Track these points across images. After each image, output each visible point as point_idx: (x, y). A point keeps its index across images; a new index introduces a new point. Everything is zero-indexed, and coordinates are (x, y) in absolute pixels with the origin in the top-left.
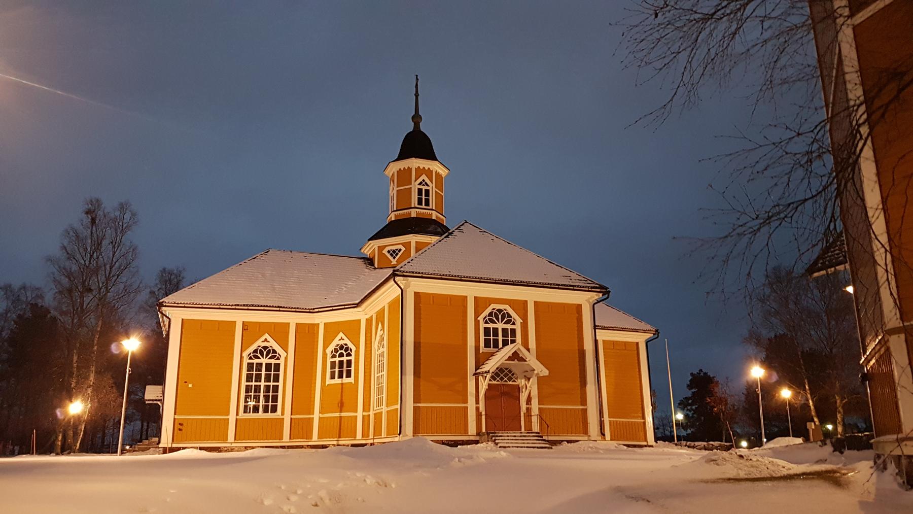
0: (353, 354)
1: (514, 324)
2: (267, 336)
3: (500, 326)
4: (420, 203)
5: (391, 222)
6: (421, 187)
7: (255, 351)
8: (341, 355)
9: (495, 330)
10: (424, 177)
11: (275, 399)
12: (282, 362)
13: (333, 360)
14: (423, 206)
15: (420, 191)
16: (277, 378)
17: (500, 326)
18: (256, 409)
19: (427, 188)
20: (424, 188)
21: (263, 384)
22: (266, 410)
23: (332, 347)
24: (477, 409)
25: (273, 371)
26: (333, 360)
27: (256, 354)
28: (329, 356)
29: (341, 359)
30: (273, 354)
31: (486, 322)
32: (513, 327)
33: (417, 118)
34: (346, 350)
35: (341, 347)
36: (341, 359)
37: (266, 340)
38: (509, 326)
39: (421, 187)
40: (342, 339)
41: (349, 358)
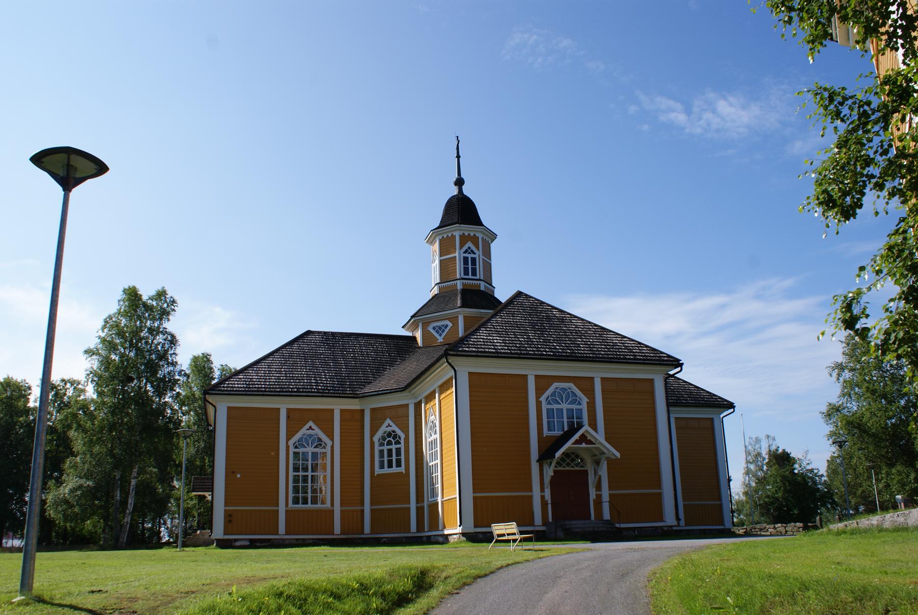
0: (402, 441)
2: (310, 424)
3: (310, 450)
6: (466, 255)
8: (389, 443)
10: (469, 244)
11: (296, 490)
13: (381, 448)
14: (470, 276)
19: (473, 256)
20: (470, 256)
21: (310, 473)
24: (543, 497)
26: (381, 448)
29: (389, 447)
30: (320, 443)
33: (460, 182)
35: (389, 435)
36: (389, 447)
37: (310, 428)
39: (466, 255)
40: (389, 425)
41: (398, 446)
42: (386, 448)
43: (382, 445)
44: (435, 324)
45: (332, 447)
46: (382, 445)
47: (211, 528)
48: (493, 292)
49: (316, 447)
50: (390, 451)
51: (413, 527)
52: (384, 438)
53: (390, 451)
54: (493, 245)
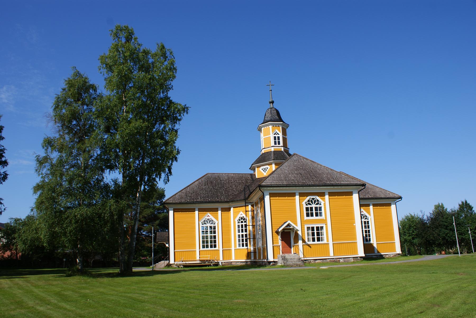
1: (320, 204)
3: (314, 206)
4: (275, 143)
5: (263, 154)
6: (275, 135)
7: (204, 221)
8: (242, 222)
9: (311, 209)
11: (203, 242)
12: (216, 225)
15: (275, 138)
16: (215, 232)
17: (314, 206)
18: (318, 228)
19: (278, 135)
20: (277, 136)
22: (211, 247)
23: (238, 218)
25: (213, 230)
27: (204, 223)
28: (237, 222)
30: (211, 221)
31: (307, 205)
32: (320, 206)
34: (242, 219)
35: (242, 219)
38: (318, 206)
39: (275, 135)
42: (240, 224)
43: (239, 223)
44: (262, 167)
45: (325, 204)
46: (239, 223)
47: (169, 260)
48: (288, 151)
49: (211, 224)
50: (242, 225)
51: (257, 258)
52: (239, 220)
53: (242, 225)
54: (287, 130)
